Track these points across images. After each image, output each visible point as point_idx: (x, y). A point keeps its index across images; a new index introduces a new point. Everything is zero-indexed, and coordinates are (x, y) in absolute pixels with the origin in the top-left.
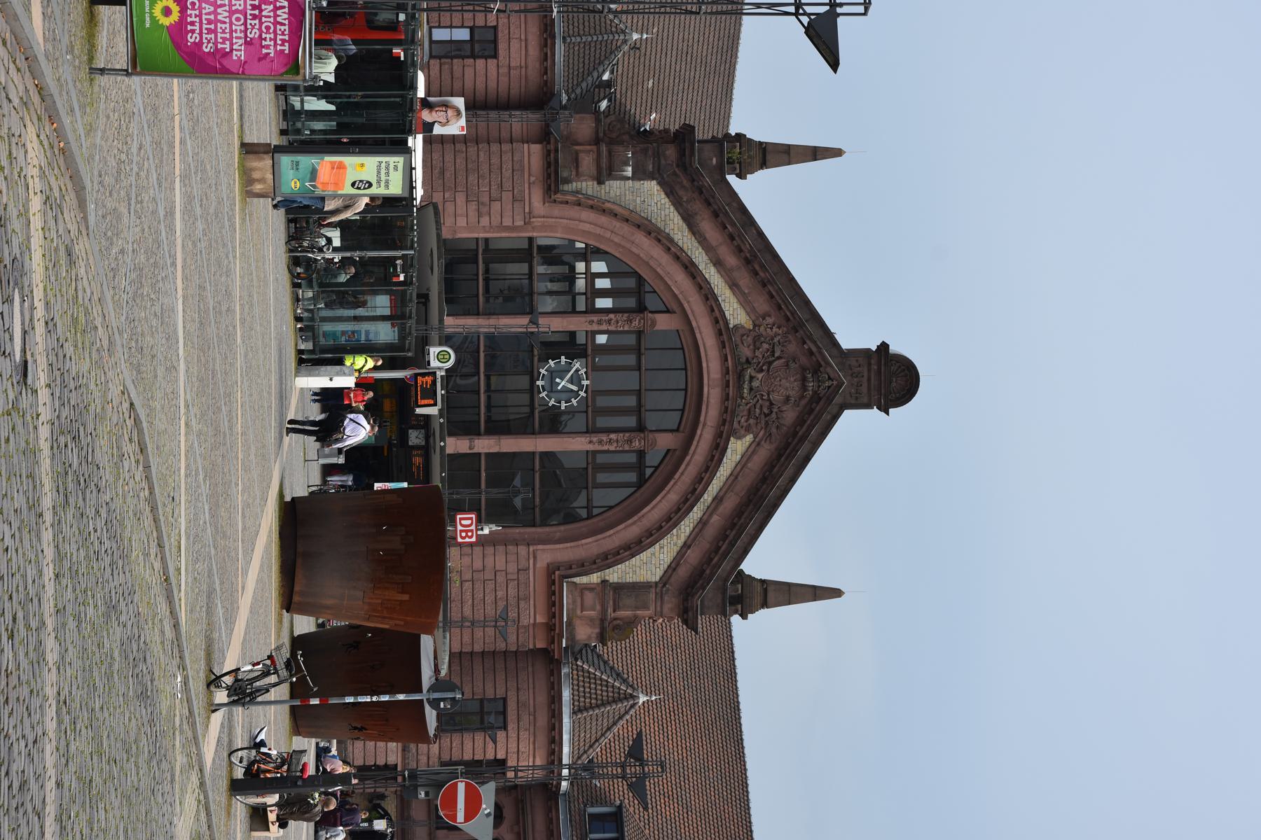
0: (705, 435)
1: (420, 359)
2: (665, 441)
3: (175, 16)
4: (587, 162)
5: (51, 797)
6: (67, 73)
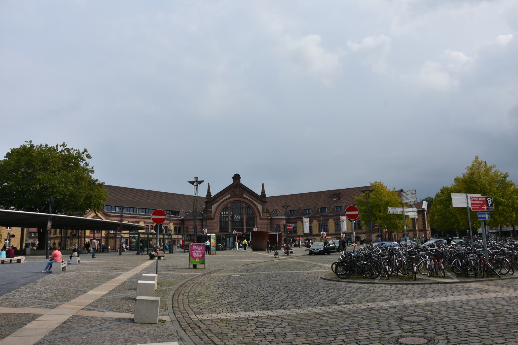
0: (244, 200)
1: (235, 234)
2: (244, 205)
3: (198, 259)
4: (209, 215)
5: (290, 272)
6: (205, 271)
